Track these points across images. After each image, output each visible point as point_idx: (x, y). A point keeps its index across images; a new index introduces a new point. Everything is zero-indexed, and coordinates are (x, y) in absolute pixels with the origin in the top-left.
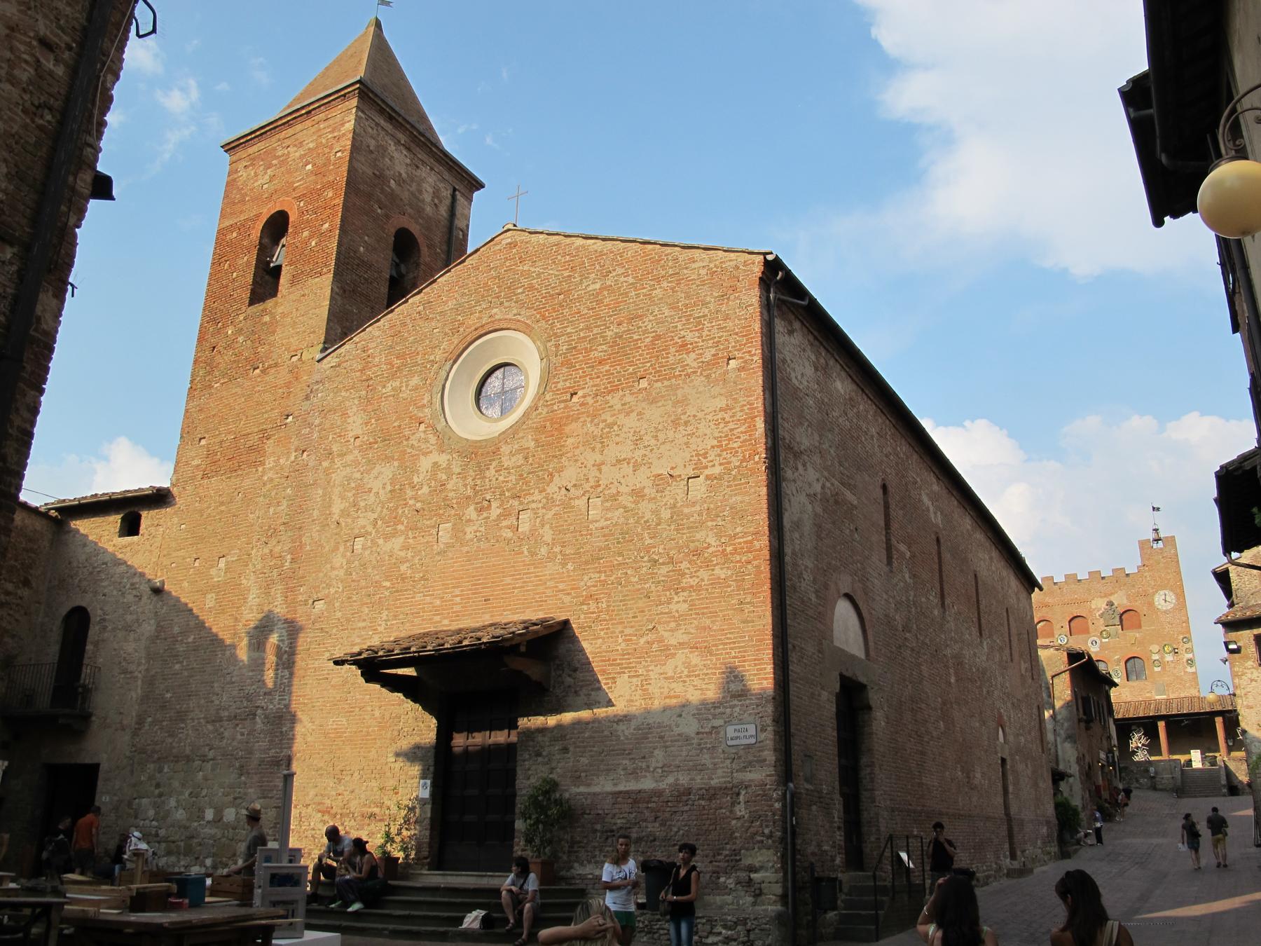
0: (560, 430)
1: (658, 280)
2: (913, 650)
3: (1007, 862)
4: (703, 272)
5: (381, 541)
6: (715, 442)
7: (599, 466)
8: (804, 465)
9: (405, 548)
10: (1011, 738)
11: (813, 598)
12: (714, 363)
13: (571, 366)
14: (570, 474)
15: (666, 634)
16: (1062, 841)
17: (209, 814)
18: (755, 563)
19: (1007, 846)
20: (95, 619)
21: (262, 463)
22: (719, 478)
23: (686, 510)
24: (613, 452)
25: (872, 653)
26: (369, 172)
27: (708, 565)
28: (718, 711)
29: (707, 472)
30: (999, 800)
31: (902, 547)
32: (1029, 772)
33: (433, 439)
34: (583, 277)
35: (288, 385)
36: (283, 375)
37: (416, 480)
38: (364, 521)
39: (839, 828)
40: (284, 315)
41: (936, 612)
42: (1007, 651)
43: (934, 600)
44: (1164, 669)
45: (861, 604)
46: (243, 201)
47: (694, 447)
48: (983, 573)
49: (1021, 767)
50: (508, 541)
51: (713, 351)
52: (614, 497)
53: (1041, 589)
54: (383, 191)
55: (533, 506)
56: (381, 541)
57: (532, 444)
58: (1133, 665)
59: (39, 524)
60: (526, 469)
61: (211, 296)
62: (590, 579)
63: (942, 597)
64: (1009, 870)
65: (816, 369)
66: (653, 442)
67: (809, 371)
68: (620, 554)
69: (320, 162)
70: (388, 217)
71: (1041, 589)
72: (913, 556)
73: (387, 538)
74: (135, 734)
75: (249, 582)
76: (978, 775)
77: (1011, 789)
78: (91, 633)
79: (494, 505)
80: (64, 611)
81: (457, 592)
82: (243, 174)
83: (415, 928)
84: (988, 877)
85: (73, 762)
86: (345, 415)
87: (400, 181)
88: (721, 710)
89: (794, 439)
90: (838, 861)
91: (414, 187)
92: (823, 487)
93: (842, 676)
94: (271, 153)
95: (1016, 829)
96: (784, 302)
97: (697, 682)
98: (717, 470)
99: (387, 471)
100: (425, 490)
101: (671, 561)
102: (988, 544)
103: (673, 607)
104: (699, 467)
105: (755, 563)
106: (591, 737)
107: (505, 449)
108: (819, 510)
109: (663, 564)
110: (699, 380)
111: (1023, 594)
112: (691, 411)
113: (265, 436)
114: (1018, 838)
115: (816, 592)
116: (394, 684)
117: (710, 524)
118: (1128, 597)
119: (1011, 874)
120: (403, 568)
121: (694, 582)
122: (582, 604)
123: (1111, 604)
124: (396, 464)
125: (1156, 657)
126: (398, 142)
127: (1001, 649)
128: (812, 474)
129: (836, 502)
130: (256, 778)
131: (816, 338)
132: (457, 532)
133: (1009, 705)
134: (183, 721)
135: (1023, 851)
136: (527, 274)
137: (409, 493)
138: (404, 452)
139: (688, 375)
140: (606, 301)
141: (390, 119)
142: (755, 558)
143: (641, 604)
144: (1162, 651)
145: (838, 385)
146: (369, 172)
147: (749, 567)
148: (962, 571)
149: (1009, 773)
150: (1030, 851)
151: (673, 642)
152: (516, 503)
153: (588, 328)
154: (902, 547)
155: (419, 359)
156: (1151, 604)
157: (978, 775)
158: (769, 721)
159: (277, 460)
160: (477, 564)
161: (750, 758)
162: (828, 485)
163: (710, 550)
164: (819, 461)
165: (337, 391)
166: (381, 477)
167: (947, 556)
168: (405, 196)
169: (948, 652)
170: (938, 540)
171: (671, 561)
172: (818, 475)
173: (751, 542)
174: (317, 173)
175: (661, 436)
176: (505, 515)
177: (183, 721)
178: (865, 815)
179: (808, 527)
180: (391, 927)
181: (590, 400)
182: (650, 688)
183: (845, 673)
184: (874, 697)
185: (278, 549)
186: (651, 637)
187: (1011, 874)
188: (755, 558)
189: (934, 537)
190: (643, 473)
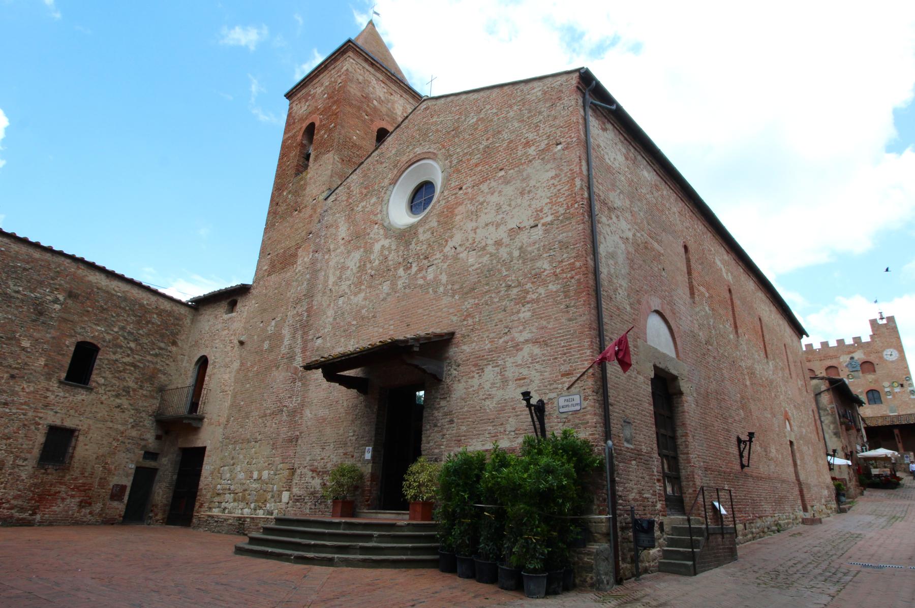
0: (452, 212)
1: (511, 106)
2: (715, 358)
3: (801, 514)
4: (539, 94)
5: (352, 297)
6: (548, 200)
7: (475, 230)
8: (617, 217)
9: (365, 299)
10: (795, 428)
11: (628, 308)
12: (548, 148)
13: (458, 171)
14: (458, 238)
15: (516, 335)
16: (838, 501)
17: (255, 475)
18: (577, 277)
19: (799, 502)
20: (210, 362)
21: (296, 262)
22: (552, 223)
23: (529, 249)
24: (484, 219)
25: (681, 355)
26: (359, 94)
27: (545, 283)
28: (552, 387)
29: (542, 221)
30: (791, 469)
31: (702, 289)
32: (811, 452)
33: (382, 232)
34: (466, 116)
35: (311, 216)
36: (308, 211)
37: (372, 257)
38: (344, 286)
39: (659, 480)
40: (310, 178)
41: (732, 336)
42: (787, 371)
43: (729, 327)
44: (894, 396)
45: (670, 320)
46: (294, 123)
47: (534, 206)
48: (765, 319)
49: (805, 449)
50: (421, 286)
51: (546, 142)
52: (484, 248)
53: (807, 336)
54: (368, 106)
55: (436, 262)
56: (352, 297)
57: (436, 224)
58: (874, 396)
59: (183, 310)
60: (432, 240)
61: (278, 176)
62: (469, 303)
63: (736, 327)
64: (803, 519)
65: (627, 159)
66: (508, 208)
67: (621, 158)
68: (487, 284)
69: (330, 91)
70: (372, 121)
71: (807, 336)
72: (711, 297)
73: (355, 295)
74: (225, 428)
75: (286, 332)
76: (773, 451)
77: (799, 462)
78: (208, 370)
79: (414, 265)
80: (196, 359)
81: (392, 322)
82: (295, 108)
83: (270, 550)
84: (788, 524)
85: (193, 446)
86: (337, 227)
87: (380, 101)
88: (555, 386)
89: (609, 198)
90: (659, 506)
91: (389, 105)
92: (634, 235)
93: (655, 366)
94: (308, 94)
95: (805, 491)
96: (595, 105)
97: (538, 366)
98: (549, 219)
99: (357, 255)
100: (377, 262)
101: (519, 284)
102: (767, 301)
103: (521, 315)
104: (538, 218)
105: (577, 277)
106: (468, 411)
107: (421, 230)
108: (631, 249)
109: (515, 287)
110: (537, 163)
111: (795, 338)
112: (532, 183)
113: (298, 247)
114: (807, 496)
115: (631, 304)
116: (347, 382)
117: (545, 255)
118: (865, 353)
119: (805, 521)
120: (364, 311)
121: (534, 296)
122: (464, 320)
123: (852, 358)
124: (362, 250)
125: (887, 390)
126: (378, 79)
127: (782, 369)
128: (623, 225)
129: (646, 248)
130: (280, 450)
131: (626, 139)
132: (393, 285)
133: (792, 406)
134: (248, 418)
135: (812, 506)
136: (435, 123)
137: (368, 266)
138: (366, 243)
139: (530, 161)
140: (480, 128)
141: (372, 65)
142: (576, 274)
143: (500, 316)
144: (891, 386)
145: (645, 173)
146: (359, 94)
147: (573, 280)
148: (749, 314)
149: (796, 451)
150: (818, 506)
151: (522, 339)
152: (426, 262)
153: (469, 146)
154: (702, 289)
155: (376, 187)
156: (881, 358)
157: (773, 451)
158: (589, 392)
159: (304, 258)
160: (404, 303)
161: (577, 421)
162: (639, 235)
163: (545, 274)
164: (630, 218)
165: (334, 214)
166: (353, 261)
167: (737, 302)
168: (384, 110)
169: (743, 364)
170: (730, 291)
171: (519, 284)
172: (629, 226)
173: (573, 263)
174: (329, 98)
175: (513, 203)
176: (420, 270)
177: (248, 418)
178: (683, 473)
179: (621, 258)
180: (296, 553)
181: (470, 190)
182: (506, 373)
183: (658, 365)
184: (684, 386)
185: (300, 311)
186: (506, 338)
187: (805, 521)
188: (576, 274)
189: (726, 287)
190: (503, 228)
